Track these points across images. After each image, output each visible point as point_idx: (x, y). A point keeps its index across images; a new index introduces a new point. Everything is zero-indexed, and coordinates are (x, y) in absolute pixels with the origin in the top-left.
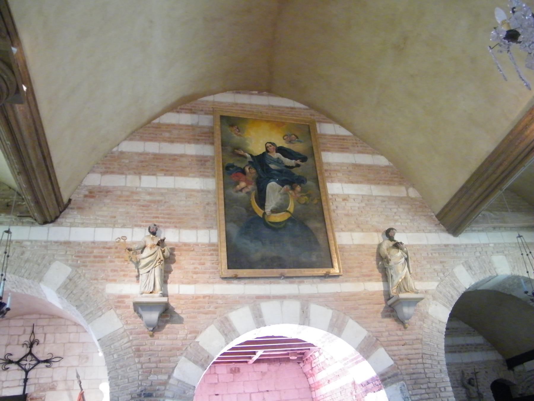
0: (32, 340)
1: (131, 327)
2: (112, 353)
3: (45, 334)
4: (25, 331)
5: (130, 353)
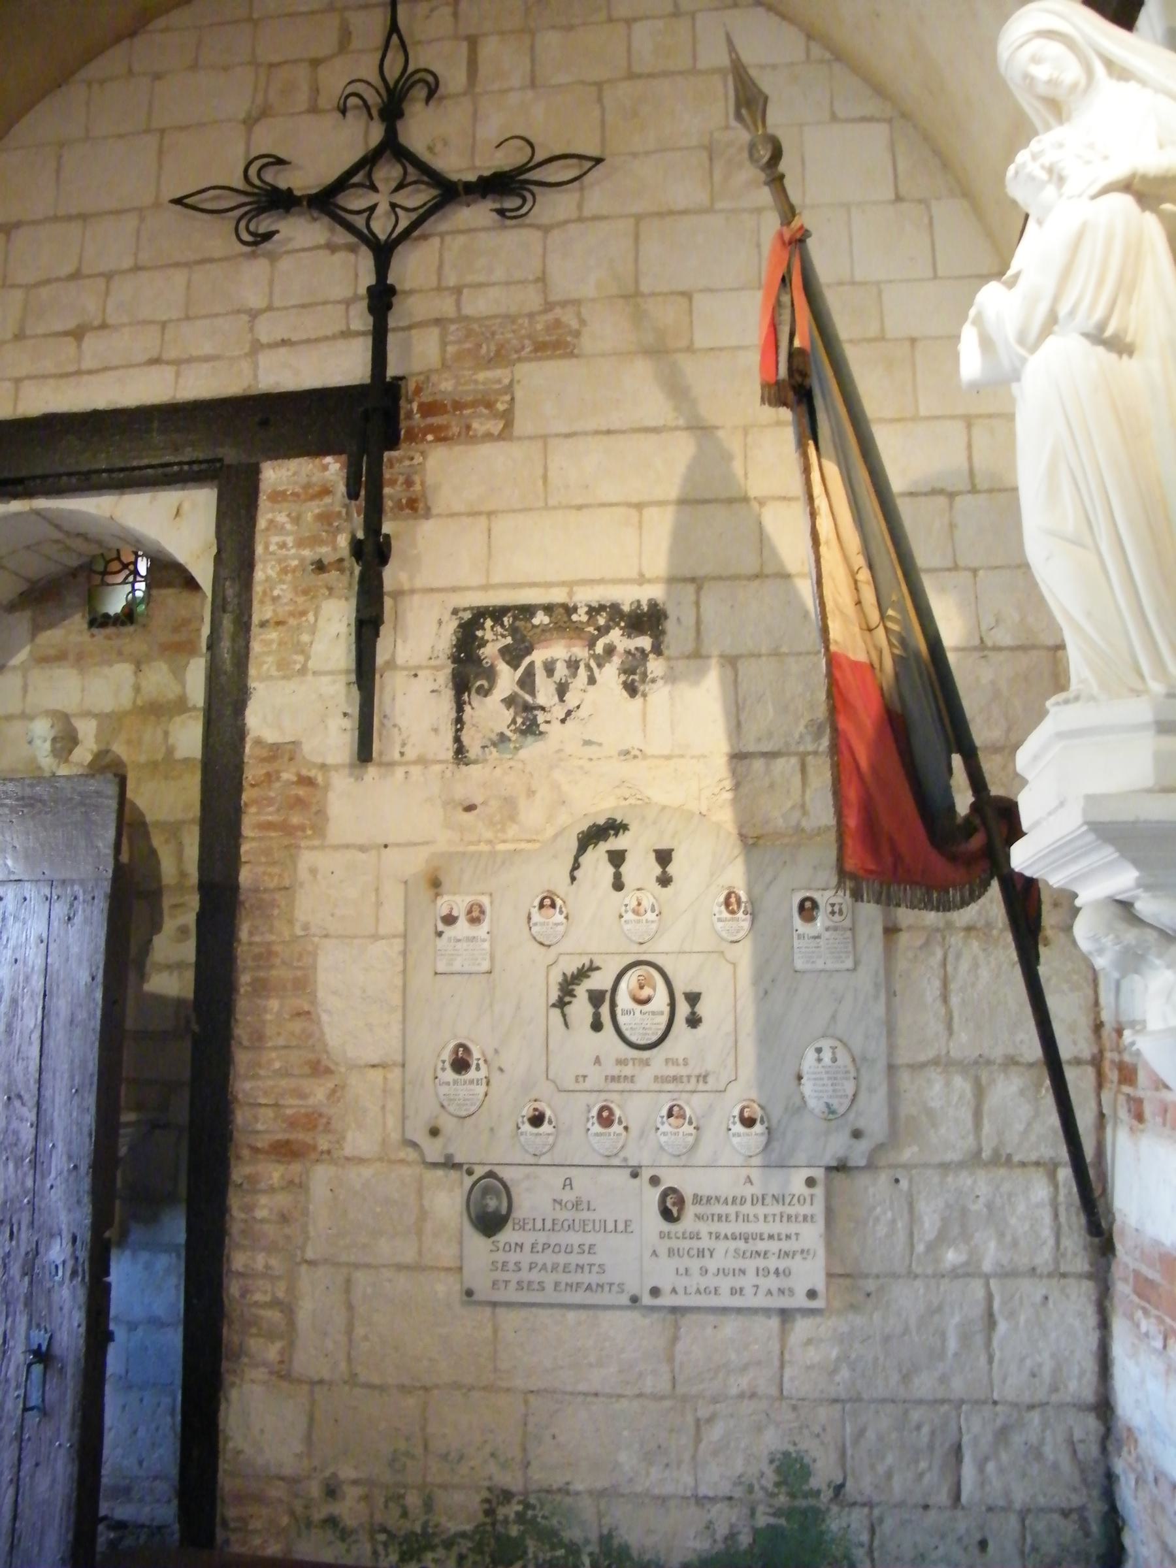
0: (393, 71)
3: (473, 42)
4: (345, 36)
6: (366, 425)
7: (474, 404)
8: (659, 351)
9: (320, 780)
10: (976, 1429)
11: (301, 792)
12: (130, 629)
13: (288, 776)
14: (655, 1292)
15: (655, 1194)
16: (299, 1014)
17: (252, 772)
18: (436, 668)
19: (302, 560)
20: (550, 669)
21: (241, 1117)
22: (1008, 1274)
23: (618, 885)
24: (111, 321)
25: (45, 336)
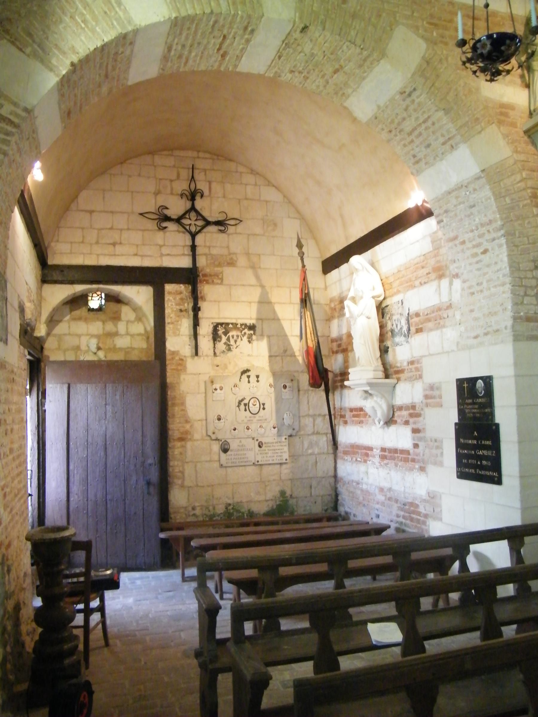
1: (522, 157)
2: (503, 194)
3: (210, 183)
5: (526, 199)
6: (190, 277)
7: (214, 275)
8: (253, 267)
9: (184, 359)
10: (314, 483)
11: (180, 362)
12: (100, 312)
13: (177, 358)
14: (258, 461)
15: (257, 443)
16: (182, 410)
17: (168, 357)
18: (209, 336)
19: (177, 309)
20: (233, 337)
21: (170, 433)
22: (319, 454)
23: (249, 382)
24: (123, 242)
25: (105, 244)
